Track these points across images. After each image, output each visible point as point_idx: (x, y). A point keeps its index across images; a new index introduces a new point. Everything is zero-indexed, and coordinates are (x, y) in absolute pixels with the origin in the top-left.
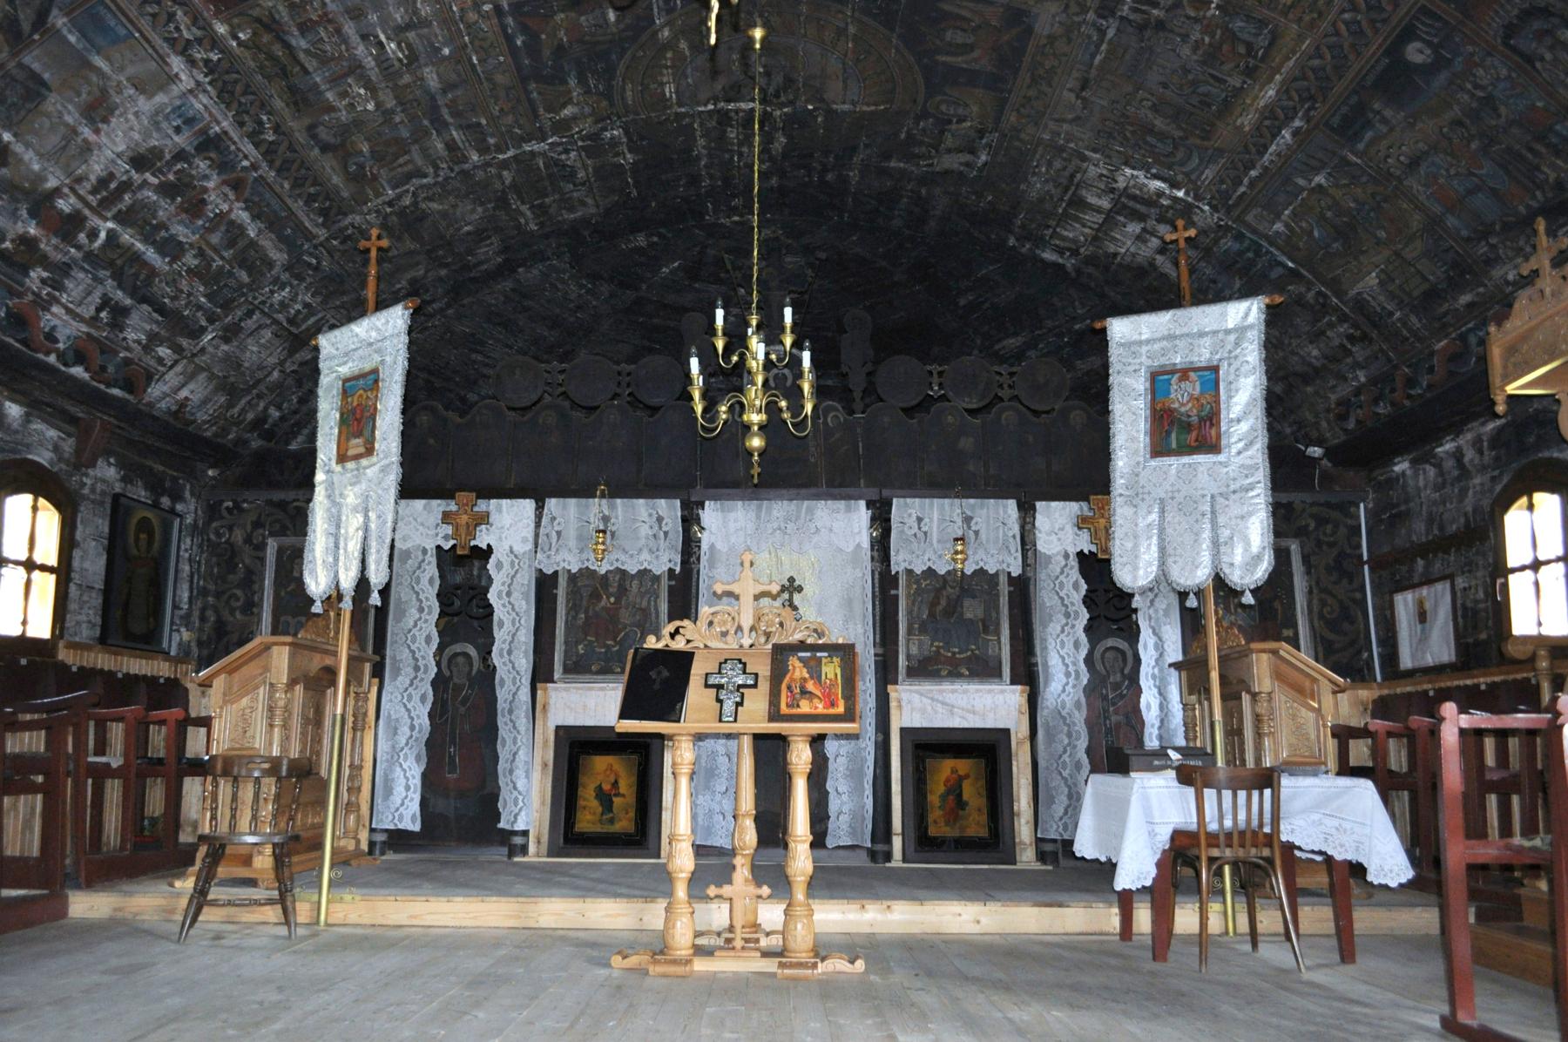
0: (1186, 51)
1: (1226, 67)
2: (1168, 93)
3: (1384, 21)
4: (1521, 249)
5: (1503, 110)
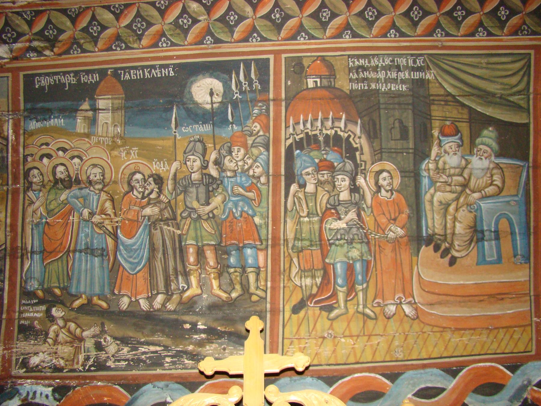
3: (217, 41)
4: (81, 339)
5: (217, 201)
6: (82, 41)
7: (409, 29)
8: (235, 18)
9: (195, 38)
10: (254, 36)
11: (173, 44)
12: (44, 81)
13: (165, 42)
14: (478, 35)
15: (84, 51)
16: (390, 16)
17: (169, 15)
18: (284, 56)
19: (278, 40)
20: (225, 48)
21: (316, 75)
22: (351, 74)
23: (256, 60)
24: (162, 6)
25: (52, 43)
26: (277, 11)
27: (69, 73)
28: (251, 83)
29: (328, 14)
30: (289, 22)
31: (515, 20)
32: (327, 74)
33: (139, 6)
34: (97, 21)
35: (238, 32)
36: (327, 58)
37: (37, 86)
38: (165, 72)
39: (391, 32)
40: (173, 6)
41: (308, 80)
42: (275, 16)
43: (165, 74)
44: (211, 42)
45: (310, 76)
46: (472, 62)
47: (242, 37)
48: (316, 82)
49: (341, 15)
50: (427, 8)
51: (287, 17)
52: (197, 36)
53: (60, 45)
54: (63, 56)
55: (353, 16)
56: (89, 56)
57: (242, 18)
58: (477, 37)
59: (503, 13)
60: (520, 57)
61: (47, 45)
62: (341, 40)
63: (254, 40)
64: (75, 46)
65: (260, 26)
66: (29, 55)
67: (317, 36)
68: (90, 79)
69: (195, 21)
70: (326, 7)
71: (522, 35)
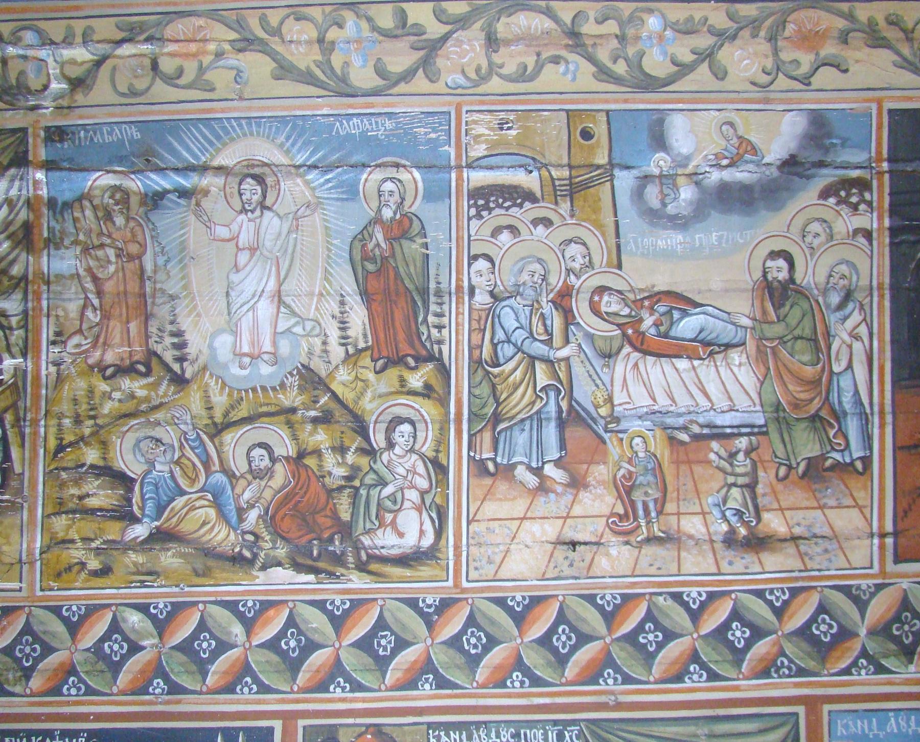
3: (175, 689)
8: (210, 645)
9: (131, 681)
10: (247, 682)
11: (90, 691)
13: (75, 686)
14: (689, 678)
16: (513, 644)
17: (86, 633)
18: (302, 723)
19: (292, 692)
20: (188, 704)
23: (245, 729)
24: (74, 616)
26: (292, 633)
29: (390, 642)
30: (314, 655)
31: (762, 647)
33: (31, 610)
35: (214, 673)
36: (386, 730)
39: (514, 678)
42: (287, 644)
44: (163, 690)
46: (677, 734)
47: (222, 683)
49: (414, 644)
50: (585, 629)
51: (311, 647)
55: (439, 646)
57: (223, 646)
58: (688, 684)
59: (738, 634)
60: (780, 720)
62: (415, 693)
63: (246, 690)
65: (256, 662)
67: (367, 684)
69: (135, 648)
70: (386, 627)
71: (780, 677)
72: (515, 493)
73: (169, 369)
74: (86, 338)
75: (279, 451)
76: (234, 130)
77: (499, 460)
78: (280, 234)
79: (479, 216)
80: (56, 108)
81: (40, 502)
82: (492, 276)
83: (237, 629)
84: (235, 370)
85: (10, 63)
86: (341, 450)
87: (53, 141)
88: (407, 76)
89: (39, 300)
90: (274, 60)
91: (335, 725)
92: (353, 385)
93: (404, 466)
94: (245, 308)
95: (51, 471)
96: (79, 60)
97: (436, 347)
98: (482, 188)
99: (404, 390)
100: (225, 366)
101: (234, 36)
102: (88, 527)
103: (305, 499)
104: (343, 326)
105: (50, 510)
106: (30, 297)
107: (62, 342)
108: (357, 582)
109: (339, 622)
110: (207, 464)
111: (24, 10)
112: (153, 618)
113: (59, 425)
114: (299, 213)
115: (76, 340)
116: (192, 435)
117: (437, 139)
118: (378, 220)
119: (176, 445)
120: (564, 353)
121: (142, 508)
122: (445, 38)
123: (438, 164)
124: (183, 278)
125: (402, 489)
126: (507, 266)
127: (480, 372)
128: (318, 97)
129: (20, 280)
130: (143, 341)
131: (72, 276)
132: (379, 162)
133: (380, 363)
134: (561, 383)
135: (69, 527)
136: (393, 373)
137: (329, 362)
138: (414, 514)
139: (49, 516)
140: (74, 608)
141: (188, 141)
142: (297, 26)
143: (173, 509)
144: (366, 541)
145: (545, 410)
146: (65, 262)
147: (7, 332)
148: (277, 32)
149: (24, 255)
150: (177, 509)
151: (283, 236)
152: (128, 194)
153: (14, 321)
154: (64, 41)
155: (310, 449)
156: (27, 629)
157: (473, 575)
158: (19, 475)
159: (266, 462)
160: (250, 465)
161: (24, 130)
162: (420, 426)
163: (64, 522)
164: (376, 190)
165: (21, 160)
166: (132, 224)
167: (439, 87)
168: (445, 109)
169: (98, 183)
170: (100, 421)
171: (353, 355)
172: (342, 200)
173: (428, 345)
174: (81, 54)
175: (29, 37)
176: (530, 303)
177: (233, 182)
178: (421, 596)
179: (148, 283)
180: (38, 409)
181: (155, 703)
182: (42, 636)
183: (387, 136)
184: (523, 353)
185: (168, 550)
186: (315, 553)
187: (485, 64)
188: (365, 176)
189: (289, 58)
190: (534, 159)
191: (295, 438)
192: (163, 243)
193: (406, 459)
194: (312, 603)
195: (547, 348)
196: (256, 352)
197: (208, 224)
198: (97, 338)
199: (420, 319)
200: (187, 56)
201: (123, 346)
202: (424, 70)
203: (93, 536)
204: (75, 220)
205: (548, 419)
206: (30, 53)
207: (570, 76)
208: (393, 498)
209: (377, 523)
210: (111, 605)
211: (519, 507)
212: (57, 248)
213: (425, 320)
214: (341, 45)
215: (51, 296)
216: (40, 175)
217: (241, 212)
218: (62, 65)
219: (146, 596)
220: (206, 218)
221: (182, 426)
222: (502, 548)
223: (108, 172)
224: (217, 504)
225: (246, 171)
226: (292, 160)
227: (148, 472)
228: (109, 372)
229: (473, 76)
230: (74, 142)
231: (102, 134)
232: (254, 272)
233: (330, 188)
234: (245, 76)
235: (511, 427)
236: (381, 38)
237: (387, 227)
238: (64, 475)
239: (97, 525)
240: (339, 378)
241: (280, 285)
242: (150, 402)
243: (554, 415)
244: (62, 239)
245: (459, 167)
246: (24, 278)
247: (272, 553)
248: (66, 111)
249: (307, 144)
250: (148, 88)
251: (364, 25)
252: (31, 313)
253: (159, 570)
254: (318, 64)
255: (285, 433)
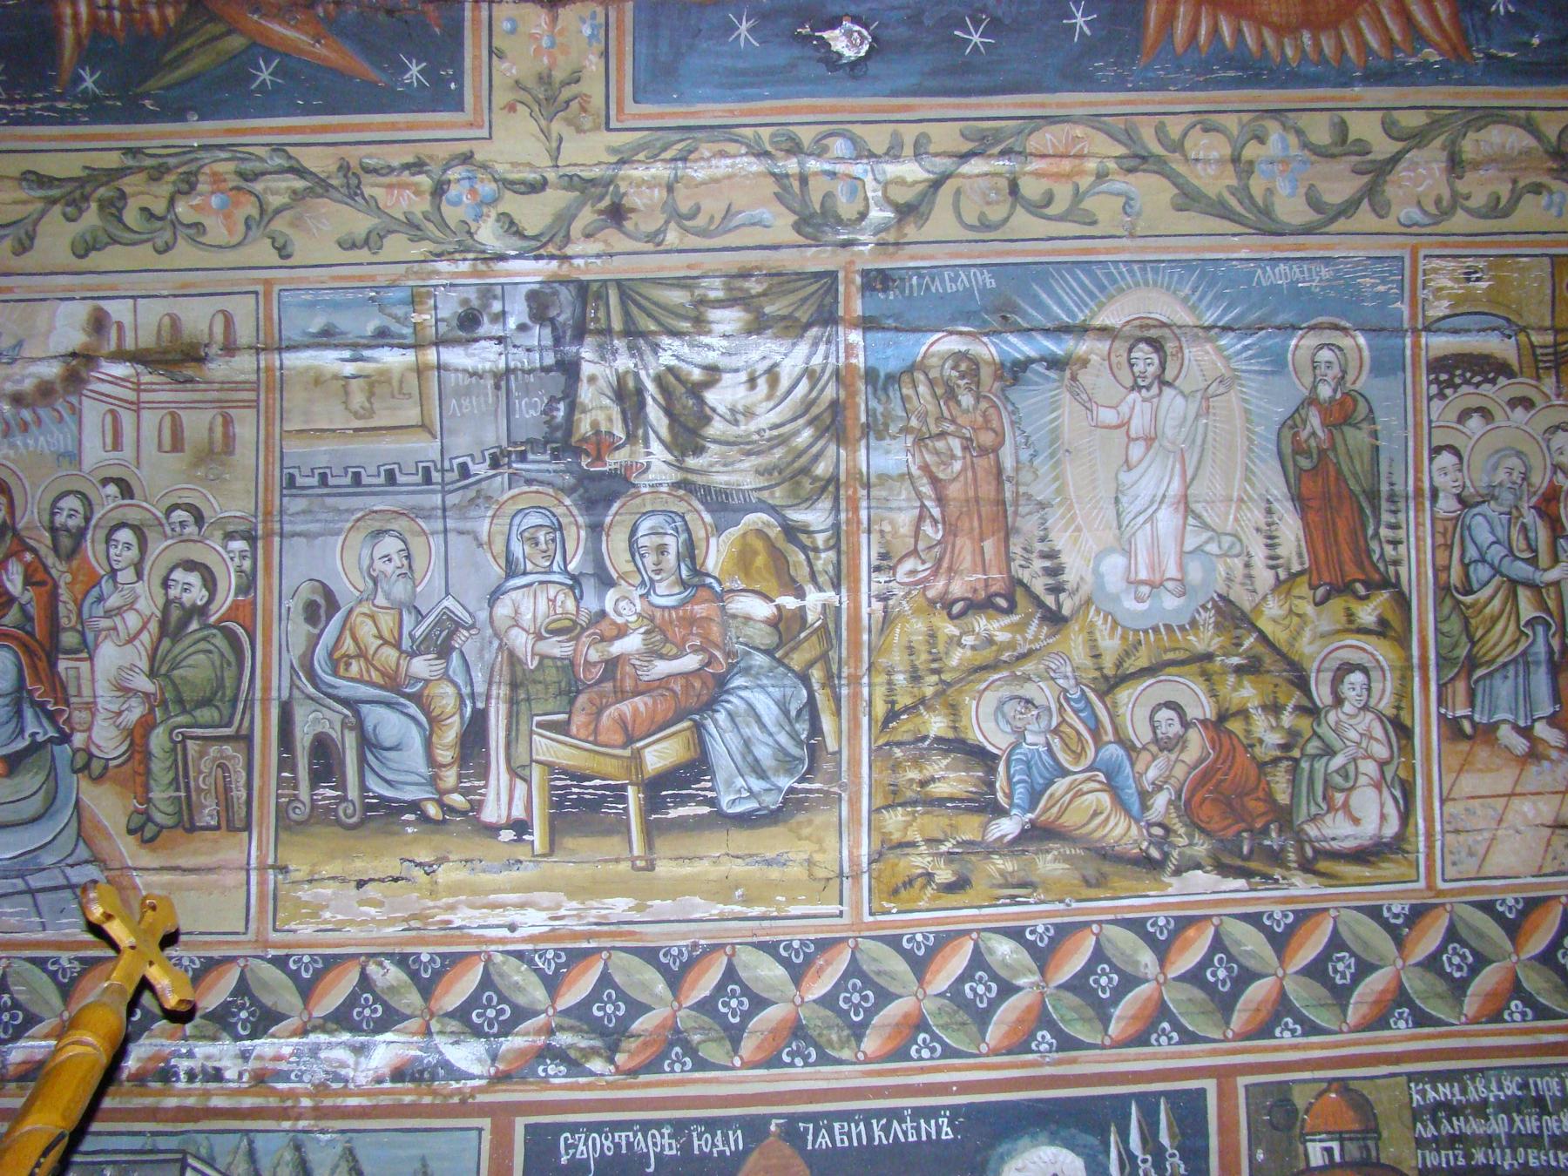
0: (530, 606)
1: (546, 747)
2: (299, 631)
3: (1067, 1043)
6: (696, 1038)
7: (1558, 997)
8: (1111, 980)
9: (1248, 1021)
11: (949, 1052)
12: (585, 1144)
13: (927, 1046)
15: (701, 1064)
16: (1507, 963)
17: (938, 971)
18: (1242, 1081)
19: (1226, 1040)
20: (1087, 1064)
21: (1328, 1133)
22: (1419, 1125)
23: (1166, 1094)
25: (612, 1039)
26: (1221, 960)
27: (658, 1124)
28: (1158, 1154)
29: (1349, 966)
32: (1356, 1127)
34: (740, 982)
35: (1119, 1018)
36: (1353, 1085)
37: (564, 1160)
38: (927, 1128)
40: (948, 949)
41: (1309, 1144)
42: (1214, 974)
43: (928, 1134)
44: (1051, 1045)
45: (1313, 1134)
47: (1131, 1031)
48: (1329, 1150)
51: (1245, 977)
52: (1013, 1030)
53: (632, 1044)
54: (642, 1078)
56: (717, 1081)
57: (1129, 982)
61: (597, 1043)
62: (1386, 1033)
63: (1163, 1039)
64: (677, 1049)
65: (1173, 1001)
66: (545, 1070)
68: (720, 1144)
69: (1007, 989)
70: (1343, 946)
72: (1498, 761)
73: (1040, 604)
74: (923, 562)
75: (1193, 713)
76: (1123, 278)
77: (1477, 718)
78: (1185, 418)
79: (1442, 395)
80: (878, 244)
81: (865, 791)
82: (1459, 475)
83: (1147, 957)
84: (1129, 603)
85: (812, 182)
86: (1274, 709)
87: (874, 289)
88: (1349, 208)
89: (856, 510)
90: (1175, 184)
91: (1286, 1082)
92: (1286, 622)
93: (1356, 729)
94: (1141, 519)
95: (880, 748)
96: (909, 179)
97: (1391, 569)
98: (1445, 357)
99: (1352, 627)
100: (1116, 599)
101: (1121, 150)
102: (934, 823)
103: (1232, 774)
104: (1271, 542)
105: (879, 802)
106: (843, 505)
107: (890, 568)
108: (1302, 887)
109: (1280, 942)
110: (1096, 732)
111: (834, 110)
112: (1031, 947)
113: (890, 683)
114: (1211, 390)
115: (909, 564)
116: (1075, 694)
117: (1386, 293)
118: (1312, 400)
119: (1054, 707)
120: (1553, 575)
121: (1010, 796)
122: (1395, 159)
123: (1387, 325)
124: (1056, 479)
125: (1355, 760)
126: (1478, 462)
127: (1448, 602)
128: (1234, 235)
129: (829, 481)
130: (1004, 565)
131: (902, 476)
132: (1313, 322)
133: (1321, 591)
134: (1551, 615)
135: (908, 824)
136: (1337, 604)
137: (1255, 591)
138: (1371, 793)
139: (878, 810)
140: (919, 938)
141: (1060, 291)
142: (1205, 140)
143: (1051, 796)
144: (1311, 830)
145: (1534, 649)
146: (891, 457)
147: (811, 554)
148: (1178, 147)
149: (832, 448)
150: (1057, 795)
151: (1189, 422)
152: (977, 364)
153: (820, 540)
154: (887, 154)
155: (1234, 709)
156: (854, 970)
157: (1451, 872)
158: (834, 753)
159: (1177, 728)
160: (1155, 733)
161: (833, 275)
162: (1375, 675)
163: (900, 818)
164: (1309, 363)
165: (828, 318)
166: (984, 405)
167: (1389, 224)
168: (1397, 253)
169: (935, 348)
170: (946, 677)
171: (1285, 581)
172: (1265, 373)
173: (1381, 566)
174: (912, 171)
175: (839, 146)
176: (1507, 509)
177: (1121, 347)
178: (1386, 903)
179: (1007, 485)
180: (858, 659)
181: (1040, 1065)
182: (876, 979)
183: (1323, 288)
184: (1502, 575)
185: (1048, 852)
186: (1246, 849)
187: (1446, 194)
188: (1293, 342)
189: (1196, 182)
190: (1508, 320)
191: (1213, 694)
192: (1028, 430)
193: (1359, 719)
194: (1244, 917)
195: (1531, 569)
196: (1158, 578)
197: (1088, 405)
198: (939, 561)
199: (1370, 532)
200: (1057, 176)
201: (975, 572)
202: (1372, 205)
203: (941, 836)
204: (904, 399)
205: (1537, 663)
206: (840, 168)
207: (1554, 211)
208: (1343, 771)
209: (1324, 806)
210: (972, 931)
211: (1504, 780)
212: (880, 438)
213: (1376, 534)
214: (1263, 167)
215: (873, 504)
216: (855, 337)
217: (1133, 389)
218: (886, 185)
219: (1017, 916)
220: (1084, 397)
221: (1060, 682)
222: (1487, 835)
223: (951, 333)
224: (1112, 787)
225: (1139, 333)
226: (1199, 318)
227: (1015, 746)
228: (956, 609)
229: (1432, 210)
230: (902, 292)
231: (943, 282)
232: (1152, 470)
233: (1251, 357)
234: (1137, 205)
235: (1490, 674)
236: (1314, 158)
237: (1326, 409)
238: (898, 752)
239: (947, 821)
240: (1267, 612)
241: (1187, 487)
242: (1015, 649)
243: (1543, 656)
244: (886, 426)
245: (1415, 331)
246: (834, 480)
247: (1188, 851)
248: (891, 249)
249: (1218, 297)
250: (1006, 220)
251: (1292, 139)
252: (844, 527)
253: (1035, 879)
254: (1233, 191)
255: (1199, 689)
